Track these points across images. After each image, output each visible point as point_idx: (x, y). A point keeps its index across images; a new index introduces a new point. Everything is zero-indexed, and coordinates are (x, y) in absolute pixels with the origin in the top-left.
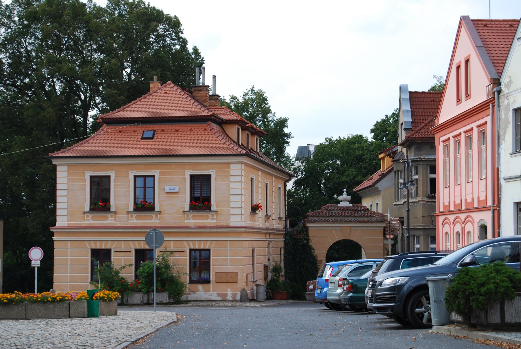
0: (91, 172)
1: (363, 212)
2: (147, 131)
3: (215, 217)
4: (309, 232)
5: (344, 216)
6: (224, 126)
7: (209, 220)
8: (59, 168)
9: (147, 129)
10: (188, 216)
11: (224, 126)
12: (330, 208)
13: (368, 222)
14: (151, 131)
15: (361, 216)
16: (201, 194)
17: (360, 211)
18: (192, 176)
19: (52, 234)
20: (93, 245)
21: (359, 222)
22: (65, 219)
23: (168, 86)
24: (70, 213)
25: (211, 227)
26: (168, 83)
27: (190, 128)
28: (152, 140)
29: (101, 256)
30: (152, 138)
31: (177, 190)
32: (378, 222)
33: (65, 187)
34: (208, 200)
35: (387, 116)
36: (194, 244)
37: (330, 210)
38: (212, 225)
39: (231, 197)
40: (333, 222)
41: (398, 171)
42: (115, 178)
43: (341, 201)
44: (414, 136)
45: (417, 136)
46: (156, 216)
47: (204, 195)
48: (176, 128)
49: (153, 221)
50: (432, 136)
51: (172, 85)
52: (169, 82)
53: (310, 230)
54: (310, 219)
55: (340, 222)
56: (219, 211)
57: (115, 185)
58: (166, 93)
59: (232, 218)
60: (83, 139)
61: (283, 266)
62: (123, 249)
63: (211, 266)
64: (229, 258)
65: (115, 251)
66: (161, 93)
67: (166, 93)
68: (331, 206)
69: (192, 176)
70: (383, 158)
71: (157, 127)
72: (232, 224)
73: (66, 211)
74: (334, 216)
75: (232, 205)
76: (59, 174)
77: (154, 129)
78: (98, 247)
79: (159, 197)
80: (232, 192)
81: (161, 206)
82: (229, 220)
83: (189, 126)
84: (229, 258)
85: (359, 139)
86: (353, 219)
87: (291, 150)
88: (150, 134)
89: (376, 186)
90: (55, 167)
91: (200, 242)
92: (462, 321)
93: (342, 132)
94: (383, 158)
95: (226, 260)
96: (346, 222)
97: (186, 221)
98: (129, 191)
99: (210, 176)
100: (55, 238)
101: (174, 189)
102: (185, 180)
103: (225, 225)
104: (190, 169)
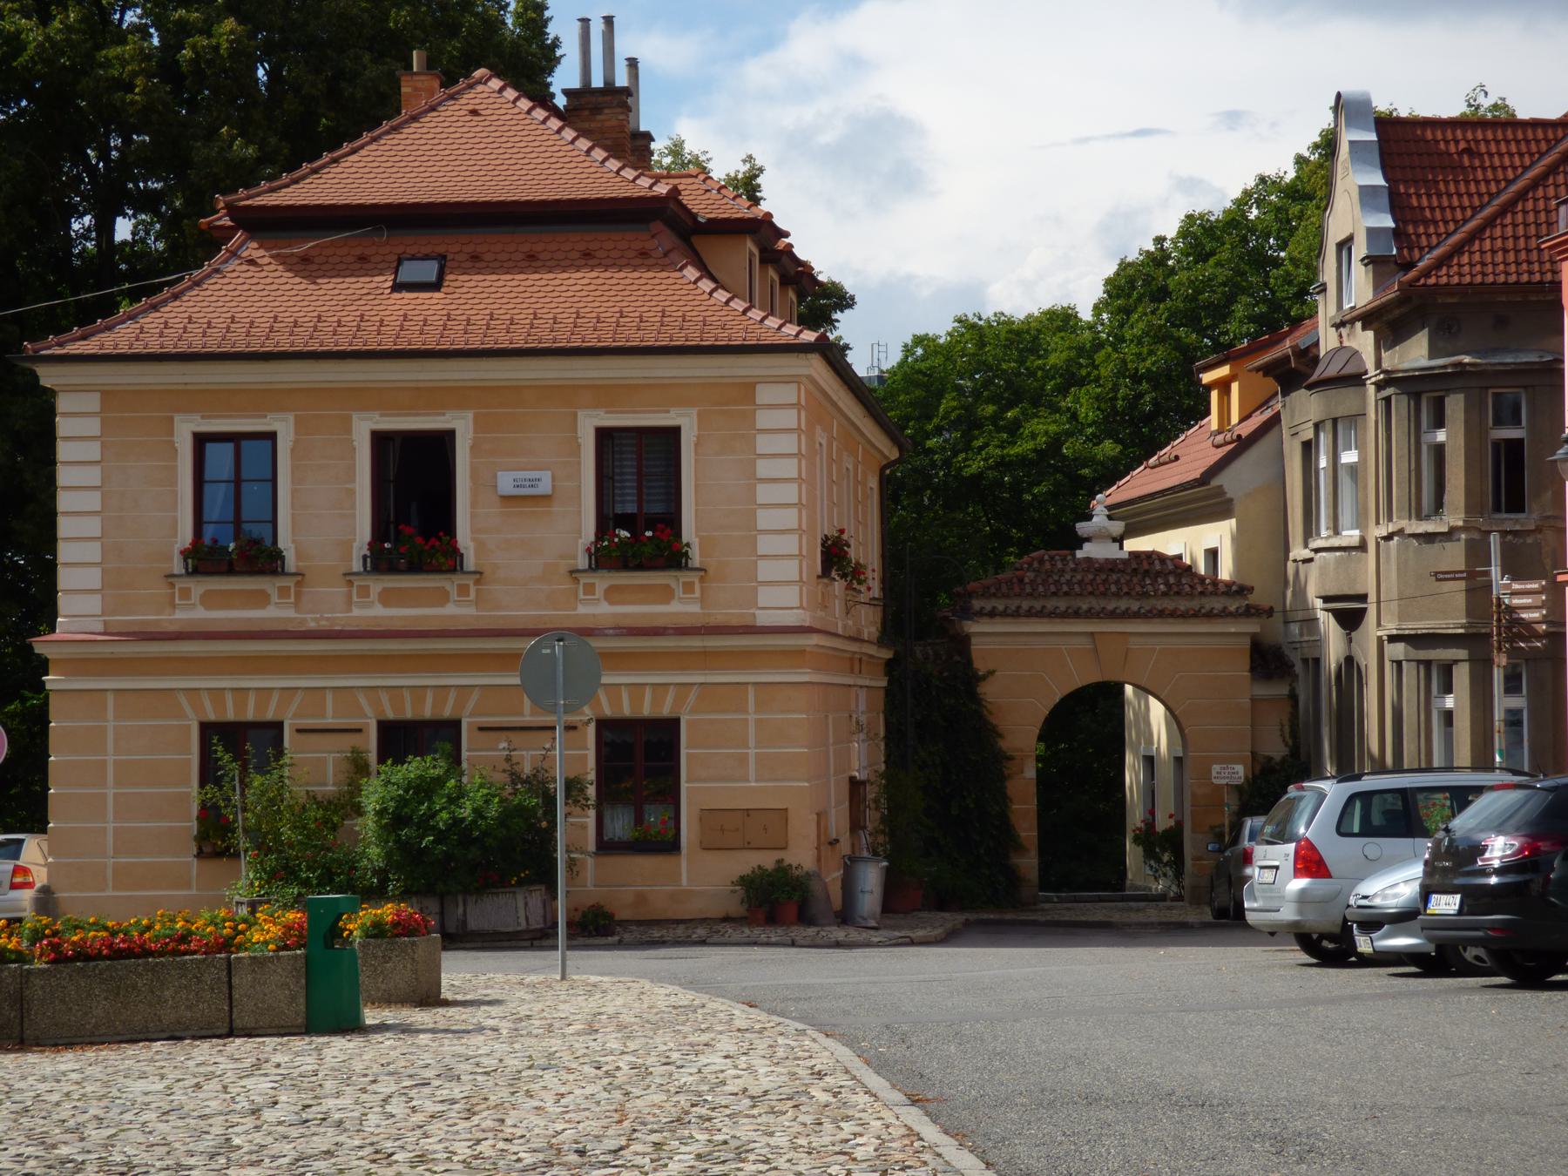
0: (197, 417)
1: (1172, 580)
2: (413, 258)
3: (697, 594)
4: (974, 655)
5: (1104, 594)
6: (695, 240)
7: (676, 601)
8: (63, 403)
9: (411, 250)
10: (590, 589)
11: (695, 240)
12: (1048, 566)
13: (1196, 615)
14: (426, 258)
15: (1165, 594)
16: (640, 507)
17: (1158, 574)
18: (604, 436)
19: (43, 666)
20: (208, 704)
21: (1161, 614)
22: (94, 604)
23: (480, 88)
24: (114, 584)
25: (683, 631)
26: (478, 73)
27: (582, 246)
28: (437, 295)
29: (235, 745)
30: (436, 286)
31: (545, 487)
32: (1231, 615)
33: (93, 476)
34: (672, 521)
35: (1160, 240)
36: (636, 700)
37: (1049, 574)
38: (687, 622)
39: (760, 513)
40: (1064, 615)
41: (1335, 421)
42: (296, 442)
43: (1088, 540)
44: (1432, 281)
45: (1444, 280)
46: (463, 590)
47: (657, 508)
48: (526, 248)
49: (450, 610)
50: (1549, 277)
51: (496, 84)
52: (480, 72)
53: (977, 646)
54: (977, 604)
55: (1090, 615)
56: (711, 571)
57: (294, 469)
58: (474, 112)
59: (765, 596)
60: (158, 288)
61: (592, 776)
62: (330, 721)
63: (684, 785)
64: (752, 752)
65: (299, 731)
66: (453, 112)
67: (474, 112)
68: (1052, 558)
69: (604, 436)
70: (1224, 385)
71: (453, 243)
72: (764, 619)
73: (97, 572)
74: (1066, 594)
75: (765, 545)
76: (63, 426)
77: (441, 249)
78: (409, 714)
79: (473, 516)
80: (764, 493)
81: (480, 546)
82: (754, 604)
83: (577, 239)
84: (752, 752)
85: (1062, 319)
86: (1135, 605)
87: (1086, 315)
88: (428, 271)
89: (1215, 482)
90: (50, 394)
91: (632, 693)
92: (746, 914)
93: (1016, 298)
94: (1224, 385)
95: (743, 760)
96: (1114, 615)
97: (582, 610)
98: (351, 493)
99: (676, 431)
100: (51, 680)
101: (534, 483)
102: (576, 450)
103: (734, 622)
104: (596, 406)
